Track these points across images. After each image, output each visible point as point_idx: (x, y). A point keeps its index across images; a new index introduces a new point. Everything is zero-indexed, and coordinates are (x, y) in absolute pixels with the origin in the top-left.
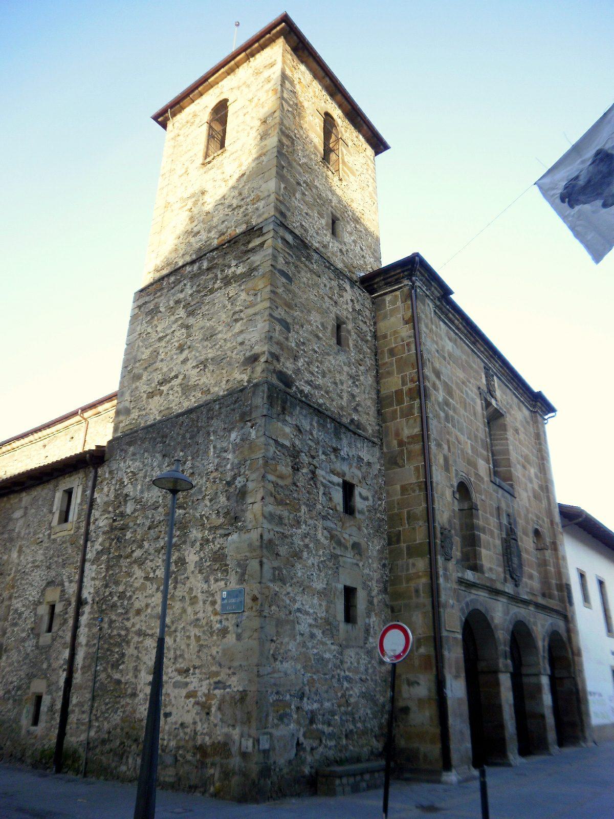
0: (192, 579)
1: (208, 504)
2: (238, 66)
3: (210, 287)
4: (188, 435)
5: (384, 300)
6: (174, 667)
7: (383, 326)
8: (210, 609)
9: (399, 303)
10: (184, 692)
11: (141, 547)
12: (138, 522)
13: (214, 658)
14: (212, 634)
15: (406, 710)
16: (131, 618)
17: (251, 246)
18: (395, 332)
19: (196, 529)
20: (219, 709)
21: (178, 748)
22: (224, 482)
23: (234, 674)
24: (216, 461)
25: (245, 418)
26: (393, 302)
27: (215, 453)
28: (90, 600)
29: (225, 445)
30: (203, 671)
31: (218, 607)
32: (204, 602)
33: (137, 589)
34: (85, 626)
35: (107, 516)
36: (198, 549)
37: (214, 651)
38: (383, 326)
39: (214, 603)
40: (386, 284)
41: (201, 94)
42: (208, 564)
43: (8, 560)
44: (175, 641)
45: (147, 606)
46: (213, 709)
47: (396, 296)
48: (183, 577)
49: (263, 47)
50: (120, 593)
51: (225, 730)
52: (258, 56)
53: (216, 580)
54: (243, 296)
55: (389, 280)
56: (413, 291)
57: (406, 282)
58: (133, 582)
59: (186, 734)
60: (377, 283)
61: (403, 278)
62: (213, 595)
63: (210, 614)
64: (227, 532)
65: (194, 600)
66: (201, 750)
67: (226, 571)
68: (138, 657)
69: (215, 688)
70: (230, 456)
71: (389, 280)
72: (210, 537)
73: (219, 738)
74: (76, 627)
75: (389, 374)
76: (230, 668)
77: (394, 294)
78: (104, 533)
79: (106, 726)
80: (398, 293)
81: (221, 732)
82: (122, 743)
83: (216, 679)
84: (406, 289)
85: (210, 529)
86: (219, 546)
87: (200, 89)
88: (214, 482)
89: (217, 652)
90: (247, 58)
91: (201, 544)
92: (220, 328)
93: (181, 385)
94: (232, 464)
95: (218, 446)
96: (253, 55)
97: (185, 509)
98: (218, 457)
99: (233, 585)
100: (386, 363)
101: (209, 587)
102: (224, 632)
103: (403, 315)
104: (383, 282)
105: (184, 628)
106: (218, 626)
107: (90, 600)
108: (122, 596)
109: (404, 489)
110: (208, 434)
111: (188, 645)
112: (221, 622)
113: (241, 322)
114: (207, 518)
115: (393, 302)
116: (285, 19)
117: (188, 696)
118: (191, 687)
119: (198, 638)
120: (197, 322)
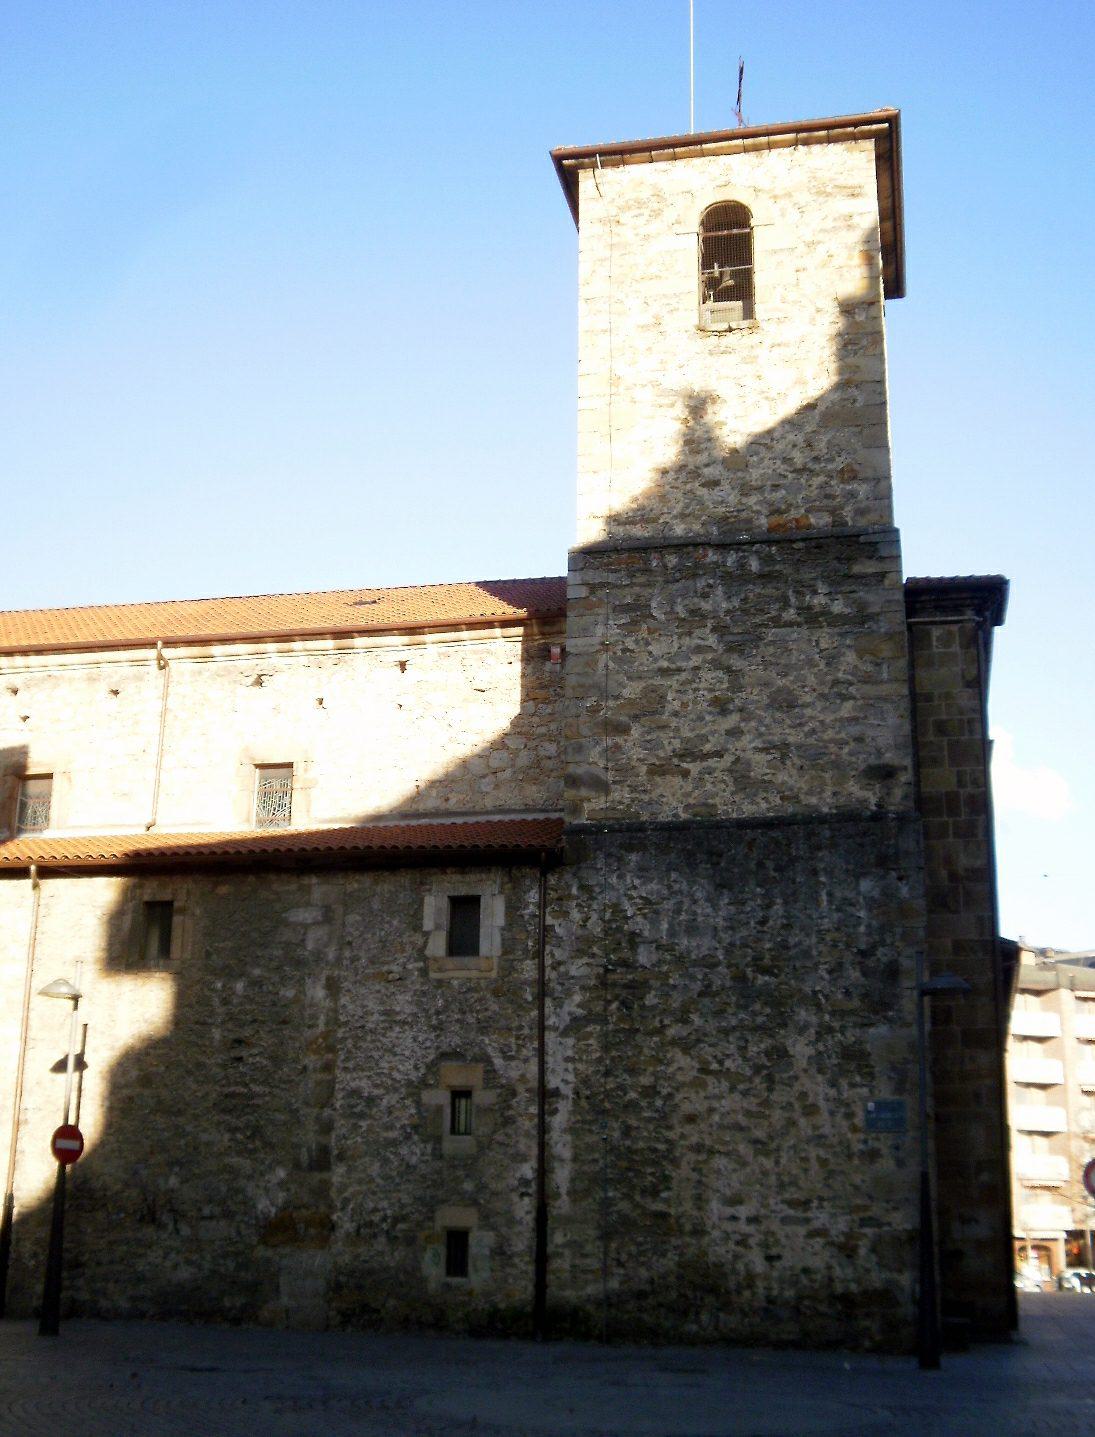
0: (804, 1079)
1: (827, 976)
2: (770, 146)
3: (774, 613)
4: (770, 864)
5: (928, 634)
6: (779, 1198)
7: (927, 678)
8: (845, 1123)
9: (956, 648)
10: (802, 1230)
11: (685, 1021)
12: (671, 981)
13: (856, 1188)
14: (850, 1156)
15: (958, 1254)
16: (677, 1126)
17: (857, 569)
18: (948, 696)
19: (807, 1010)
20: (873, 1250)
21: (800, 1298)
22: (855, 950)
23: (895, 1209)
24: (836, 916)
25: (884, 862)
26: (946, 641)
27: (830, 902)
28: (567, 1090)
29: (850, 895)
30: (837, 1203)
31: (859, 1120)
32: (832, 1113)
33: (683, 1084)
34: (564, 1131)
35: (585, 960)
36: (813, 1039)
37: (857, 1179)
38: (927, 678)
39: (849, 1116)
40: (936, 608)
41: (675, 158)
42: (835, 1062)
43: (296, 1000)
44: (777, 1163)
45: (711, 1110)
46: (862, 1251)
47: (950, 633)
48: (785, 1075)
49: (829, 140)
50: (643, 1086)
51: (886, 1275)
52: (816, 148)
53: (853, 1085)
54: (851, 657)
55: (943, 603)
56: (980, 633)
57: (969, 614)
58: (674, 1074)
59: (812, 1281)
60: (922, 602)
61: (968, 606)
62: (848, 1105)
63: (845, 1129)
64: (866, 1021)
65: (811, 1110)
66: (846, 1299)
67: (872, 1075)
68: (699, 1182)
69: (862, 1226)
70: (862, 914)
71: (943, 603)
72: (836, 1025)
73: (877, 1285)
74: (543, 1129)
75: (935, 762)
76: (888, 1202)
77: (947, 627)
78: (583, 988)
79: (643, 1273)
80: (955, 628)
81: (877, 1279)
82: (681, 1295)
83: (862, 1215)
84: (970, 626)
85: (833, 1014)
86: (853, 1039)
87: (677, 150)
88: (835, 946)
89: (863, 1181)
90: (795, 143)
91: (817, 1033)
92: (808, 699)
93: (730, 771)
94: (869, 926)
95: (838, 894)
96: (806, 143)
97: (776, 976)
98: (838, 910)
99: (885, 1092)
100: (931, 742)
101: (840, 1092)
102: (873, 1155)
103: (963, 670)
104: (933, 604)
105: (794, 1147)
106: (861, 1146)
107: (567, 1090)
108: (650, 1092)
109: (958, 947)
110: (815, 872)
111: (806, 1171)
112: (865, 1142)
113: (851, 702)
114: (826, 997)
115: (946, 641)
116: (893, 121)
117: (812, 1234)
118: (817, 1224)
119: (823, 1162)
120: (750, 668)
